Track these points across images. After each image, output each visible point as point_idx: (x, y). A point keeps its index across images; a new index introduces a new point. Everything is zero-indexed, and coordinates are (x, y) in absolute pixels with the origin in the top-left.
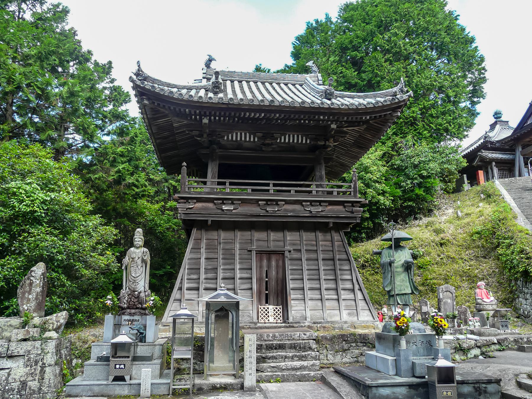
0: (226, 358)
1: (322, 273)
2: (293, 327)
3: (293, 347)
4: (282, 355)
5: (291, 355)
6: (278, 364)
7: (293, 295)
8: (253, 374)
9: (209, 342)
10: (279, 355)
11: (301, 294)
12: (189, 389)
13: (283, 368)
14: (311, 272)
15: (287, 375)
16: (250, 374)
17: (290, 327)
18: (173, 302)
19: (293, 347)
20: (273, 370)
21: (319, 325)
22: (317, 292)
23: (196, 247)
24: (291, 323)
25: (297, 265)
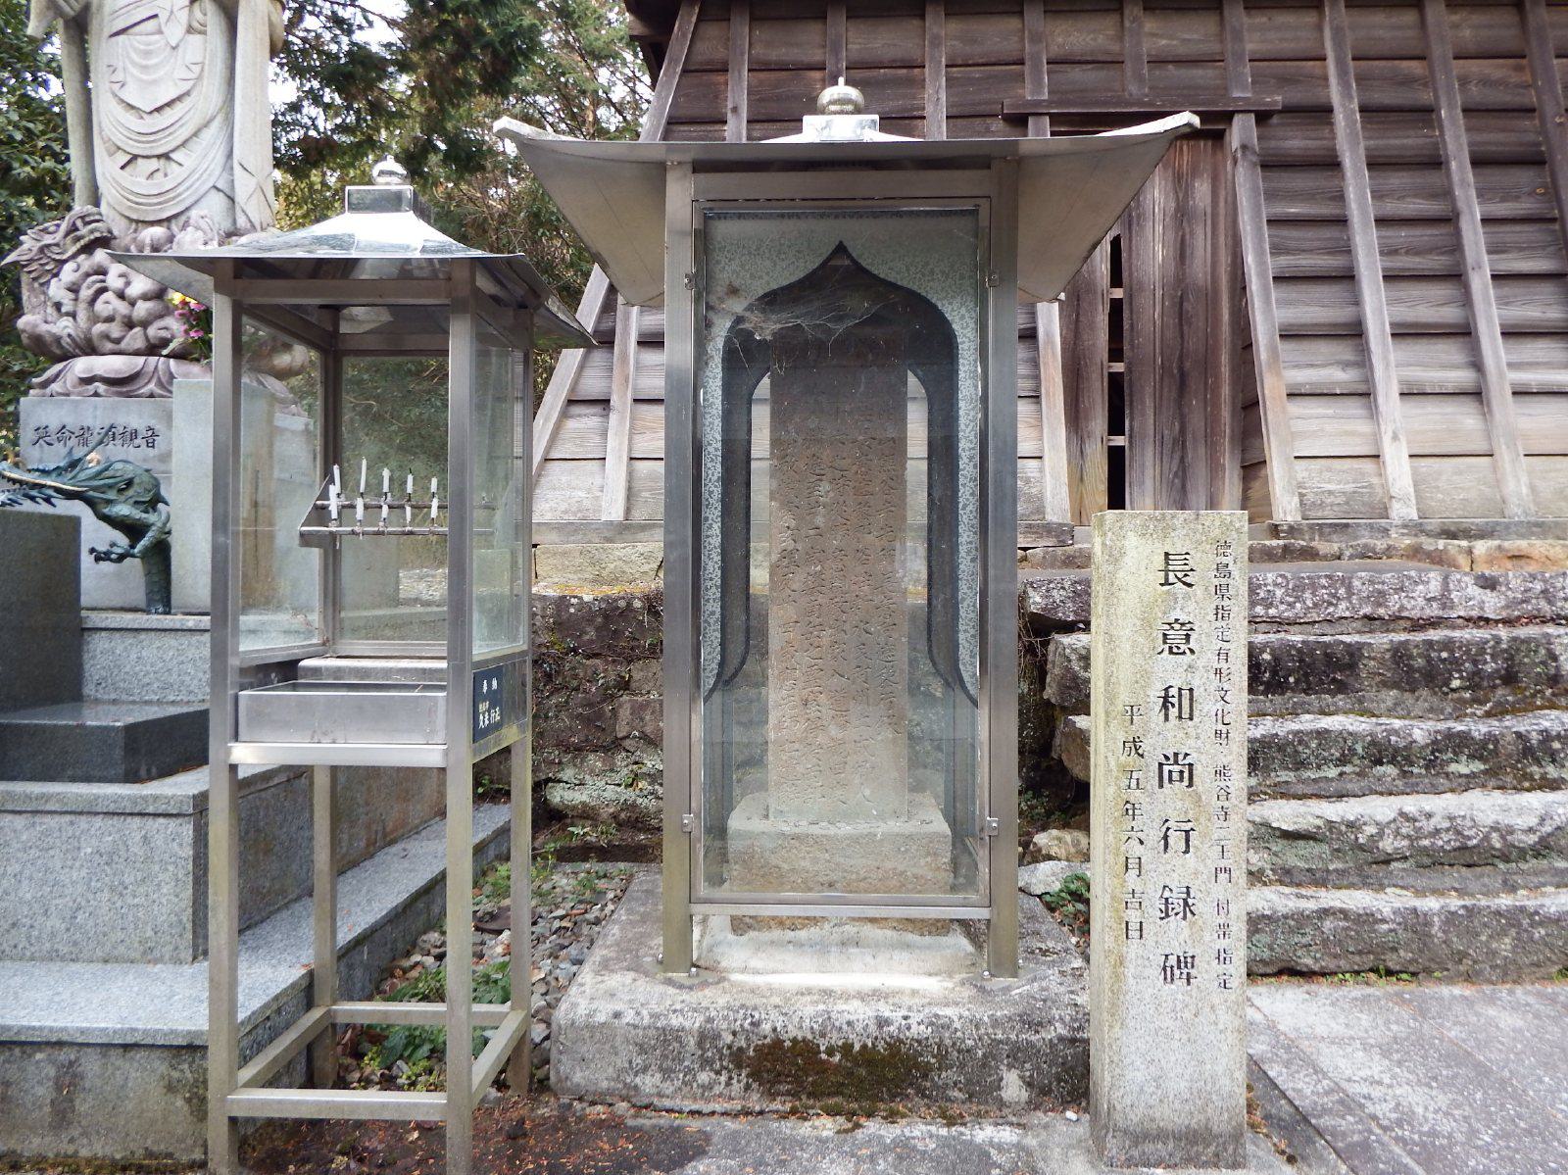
0: (877, 744)
1: (1474, 237)
2: (1309, 554)
3: (1419, 674)
4: (1343, 736)
5: (1421, 732)
6: (1334, 811)
7: (1280, 371)
8: (1207, 970)
9: (712, 606)
10: (1321, 734)
11: (1346, 365)
12: (429, 1130)
13: (1388, 844)
14: (1403, 234)
15: (1451, 918)
16: (1179, 968)
17: (1287, 553)
18: (564, 415)
19: (1419, 674)
20: (1296, 856)
21: (1481, 547)
22: (1450, 350)
23: (698, 109)
24: (1293, 530)
25: (1309, 196)
